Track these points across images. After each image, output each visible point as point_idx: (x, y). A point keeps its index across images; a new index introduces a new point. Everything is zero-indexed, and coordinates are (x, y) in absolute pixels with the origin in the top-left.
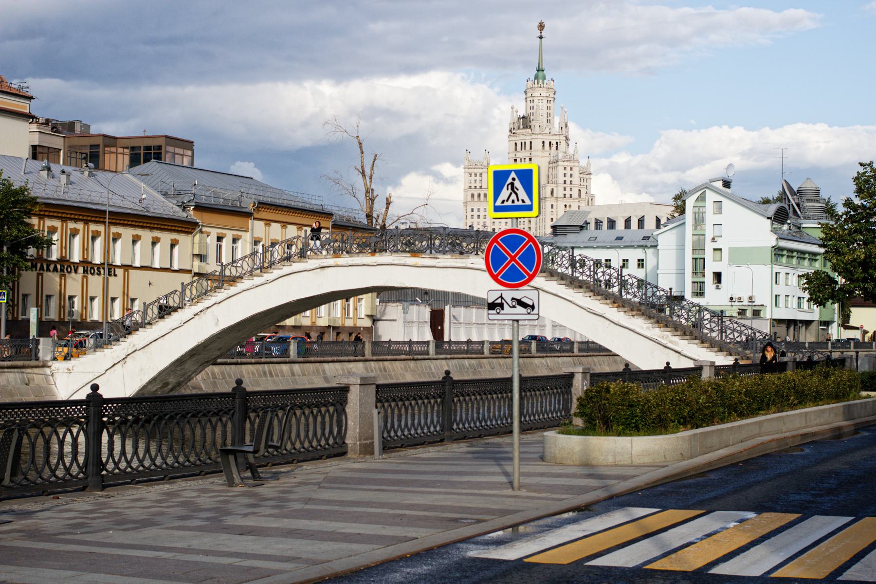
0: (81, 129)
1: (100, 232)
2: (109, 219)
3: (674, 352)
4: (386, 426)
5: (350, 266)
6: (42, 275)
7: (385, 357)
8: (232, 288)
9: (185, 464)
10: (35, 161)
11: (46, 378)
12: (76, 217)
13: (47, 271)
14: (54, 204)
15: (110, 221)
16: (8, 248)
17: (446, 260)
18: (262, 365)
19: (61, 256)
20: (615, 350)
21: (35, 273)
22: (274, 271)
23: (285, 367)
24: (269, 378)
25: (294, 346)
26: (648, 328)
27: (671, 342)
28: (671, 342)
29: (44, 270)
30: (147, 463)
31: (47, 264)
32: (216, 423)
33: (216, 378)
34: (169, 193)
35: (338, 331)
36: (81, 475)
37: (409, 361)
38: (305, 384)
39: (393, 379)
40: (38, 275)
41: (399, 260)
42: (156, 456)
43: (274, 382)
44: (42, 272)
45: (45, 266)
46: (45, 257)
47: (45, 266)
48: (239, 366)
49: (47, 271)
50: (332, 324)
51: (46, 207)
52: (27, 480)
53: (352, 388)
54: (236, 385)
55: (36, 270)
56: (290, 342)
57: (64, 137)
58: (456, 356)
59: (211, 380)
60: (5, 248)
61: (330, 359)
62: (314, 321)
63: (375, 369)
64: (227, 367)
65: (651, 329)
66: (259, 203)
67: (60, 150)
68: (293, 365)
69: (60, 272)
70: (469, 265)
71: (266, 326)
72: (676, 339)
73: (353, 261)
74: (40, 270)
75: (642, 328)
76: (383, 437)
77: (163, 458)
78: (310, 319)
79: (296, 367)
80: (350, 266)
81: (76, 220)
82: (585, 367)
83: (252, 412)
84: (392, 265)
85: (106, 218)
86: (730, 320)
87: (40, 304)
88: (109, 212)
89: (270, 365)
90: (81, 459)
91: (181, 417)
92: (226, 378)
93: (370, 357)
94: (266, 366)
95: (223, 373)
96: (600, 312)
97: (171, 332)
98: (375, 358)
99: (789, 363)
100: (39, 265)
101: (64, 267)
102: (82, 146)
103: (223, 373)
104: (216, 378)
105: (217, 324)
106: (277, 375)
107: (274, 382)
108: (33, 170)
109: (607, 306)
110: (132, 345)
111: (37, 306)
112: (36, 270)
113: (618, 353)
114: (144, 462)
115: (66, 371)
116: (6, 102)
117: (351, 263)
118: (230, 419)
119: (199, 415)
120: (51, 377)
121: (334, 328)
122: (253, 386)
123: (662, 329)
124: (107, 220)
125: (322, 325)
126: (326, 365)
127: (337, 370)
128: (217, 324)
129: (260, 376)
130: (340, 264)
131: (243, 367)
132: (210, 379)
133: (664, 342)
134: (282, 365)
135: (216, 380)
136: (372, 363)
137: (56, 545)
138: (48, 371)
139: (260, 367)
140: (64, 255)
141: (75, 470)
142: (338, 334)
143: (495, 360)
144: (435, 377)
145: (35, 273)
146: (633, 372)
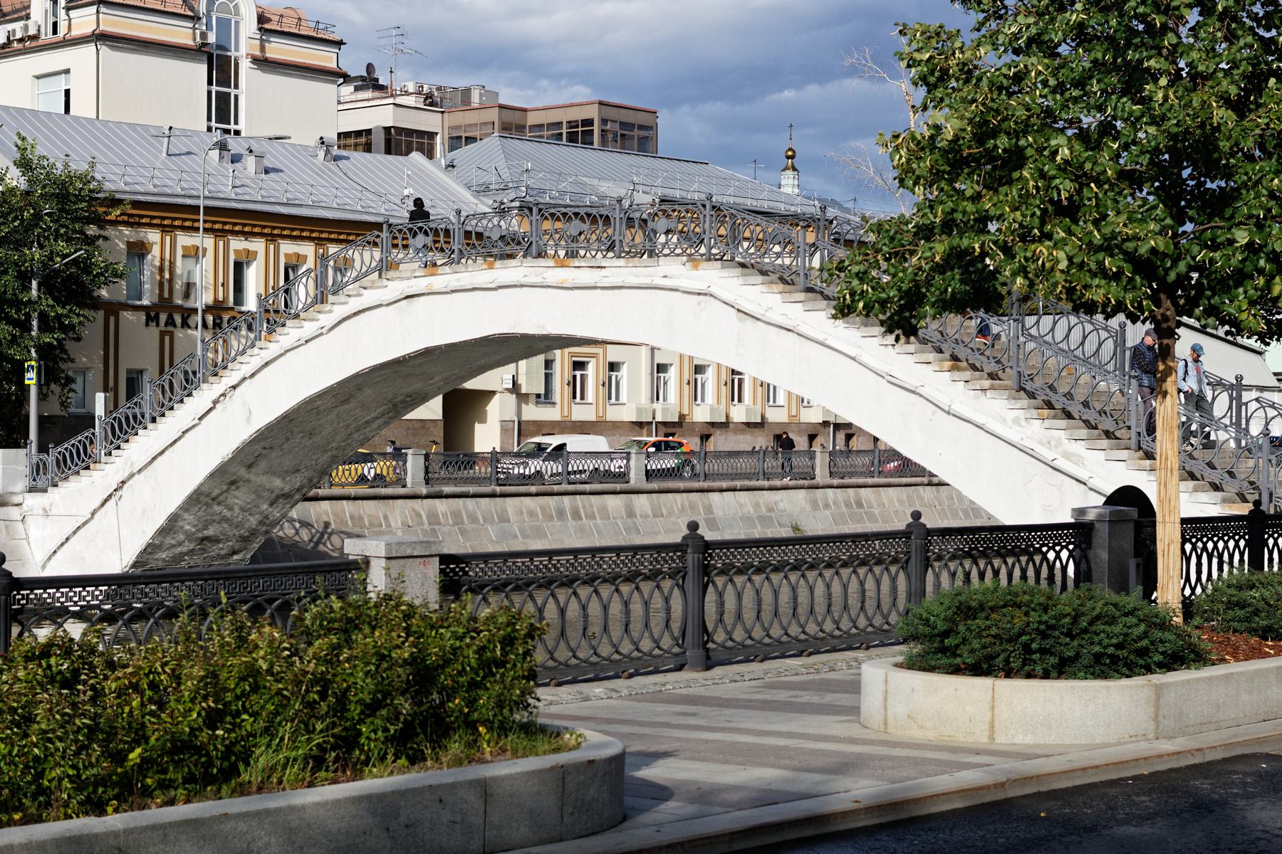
0: (481, 98)
1: (306, 257)
2: (205, 221)
3: (1074, 482)
4: (1188, 579)
5: (453, 291)
6: (171, 334)
7: (861, 481)
8: (271, 345)
9: (654, 653)
10: (389, 157)
11: (7, 527)
12: (247, 229)
13: (182, 327)
14: (142, 202)
15: (207, 226)
16: (39, 285)
17: (618, 270)
18: (556, 498)
19: (216, 300)
20: (943, 476)
21: (154, 332)
22: (335, 307)
23: (613, 502)
24: (571, 523)
25: (414, 461)
26: (1016, 421)
27: (1067, 455)
28: (1067, 455)
29: (175, 326)
30: (845, 624)
31: (183, 316)
32: (1013, 565)
33: (439, 524)
34: (492, 187)
35: (850, 432)
36: (676, 650)
37: (920, 488)
38: (656, 533)
39: (877, 521)
40: (162, 334)
41: (537, 275)
42: (734, 627)
43: (582, 530)
44: (171, 328)
45: (178, 319)
46: (179, 301)
47: (178, 319)
48: (498, 499)
49: (182, 327)
50: (832, 420)
51: (134, 208)
52: (598, 656)
53: (373, 563)
54: (911, 520)
55: (158, 325)
56: (406, 454)
57: (443, 112)
58: (738, 484)
59: (426, 526)
60: (34, 284)
61: (724, 484)
62: (794, 414)
63: (835, 503)
64: (469, 502)
65: (1023, 422)
66: (662, 201)
67: (437, 134)
68: (633, 496)
69: (214, 328)
70: (659, 281)
71: (375, 425)
72: (1079, 448)
73: (458, 280)
74: (166, 325)
75: (1004, 421)
76: (1183, 595)
77: (868, 619)
78: (786, 409)
79: (641, 502)
80: (453, 291)
81: (247, 235)
82: (393, 539)
83: (717, 575)
84: (522, 286)
85: (199, 220)
86: (1257, 400)
87: (111, 384)
88: (204, 207)
89: (578, 497)
90: (676, 626)
91: (601, 582)
92: (463, 523)
93: (829, 481)
94: (566, 499)
95: (456, 515)
96: (911, 382)
97: (180, 438)
98: (836, 482)
99: (1097, 525)
100: (163, 317)
101: (221, 319)
102: (471, 125)
103: (456, 515)
104: (439, 524)
105: (248, 420)
106: (592, 517)
107: (582, 530)
108: (195, 150)
109: (929, 368)
110: (129, 464)
111: (105, 390)
112: (158, 325)
113: (947, 480)
114: (641, 643)
115: (41, 512)
116: (290, 51)
117: (454, 285)
118: (902, 568)
119: (750, 572)
120: (20, 524)
121: (838, 427)
122: (525, 536)
123: (1047, 423)
124: (201, 225)
125: (813, 421)
126: (715, 497)
127: (741, 506)
128: (248, 420)
129: (551, 518)
130: (436, 288)
131: (509, 500)
132: (422, 524)
133: (1048, 455)
134: (606, 496)
135: (436, 527)
136: (830, 491)
137: (244, 809)
138: (14, 513)
139: (551, 501)
140: (221, 298)
141: (893, 618)
142: (849, 437)
143: (441, 506)
144: (877, 521)
145: (154, 332)
146: (18, 579)
